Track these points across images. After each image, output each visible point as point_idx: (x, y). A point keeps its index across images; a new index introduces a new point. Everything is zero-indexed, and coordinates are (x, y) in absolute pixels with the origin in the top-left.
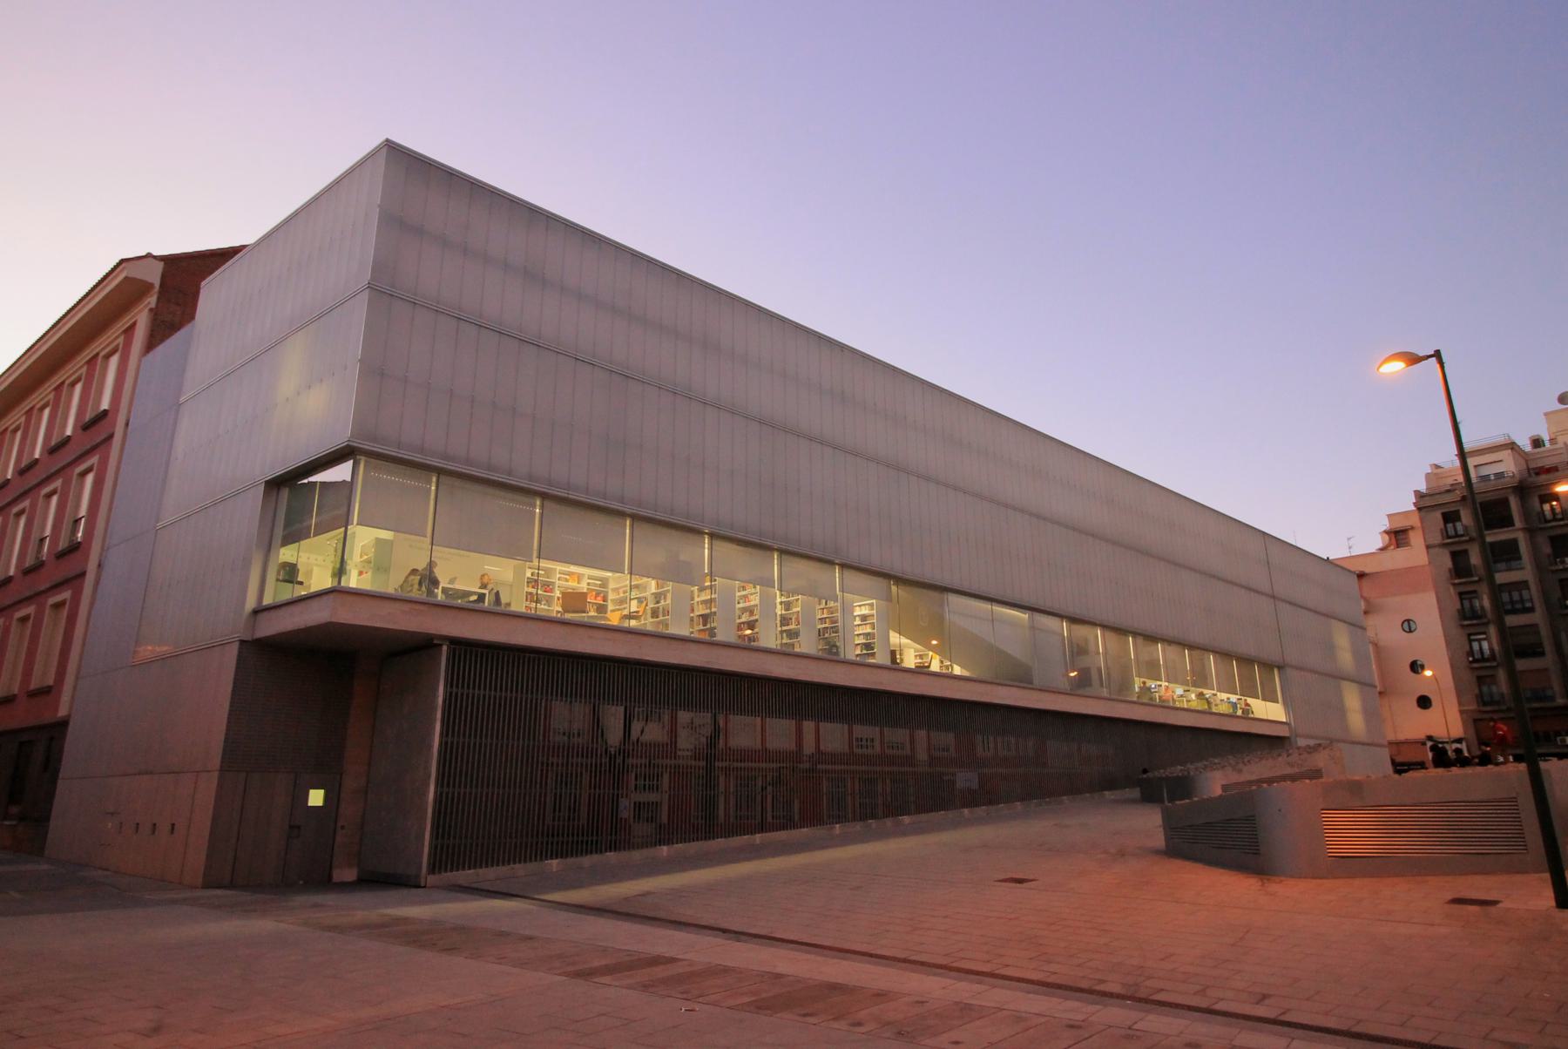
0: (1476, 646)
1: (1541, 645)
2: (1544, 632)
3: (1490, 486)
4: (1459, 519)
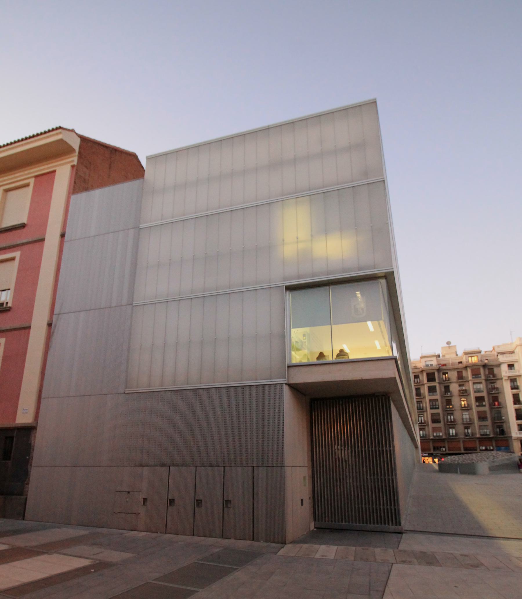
0: (420, 418)
1: (440, 419)
2: (441, 415)
3: (431, 368)
4: (419, 378)
